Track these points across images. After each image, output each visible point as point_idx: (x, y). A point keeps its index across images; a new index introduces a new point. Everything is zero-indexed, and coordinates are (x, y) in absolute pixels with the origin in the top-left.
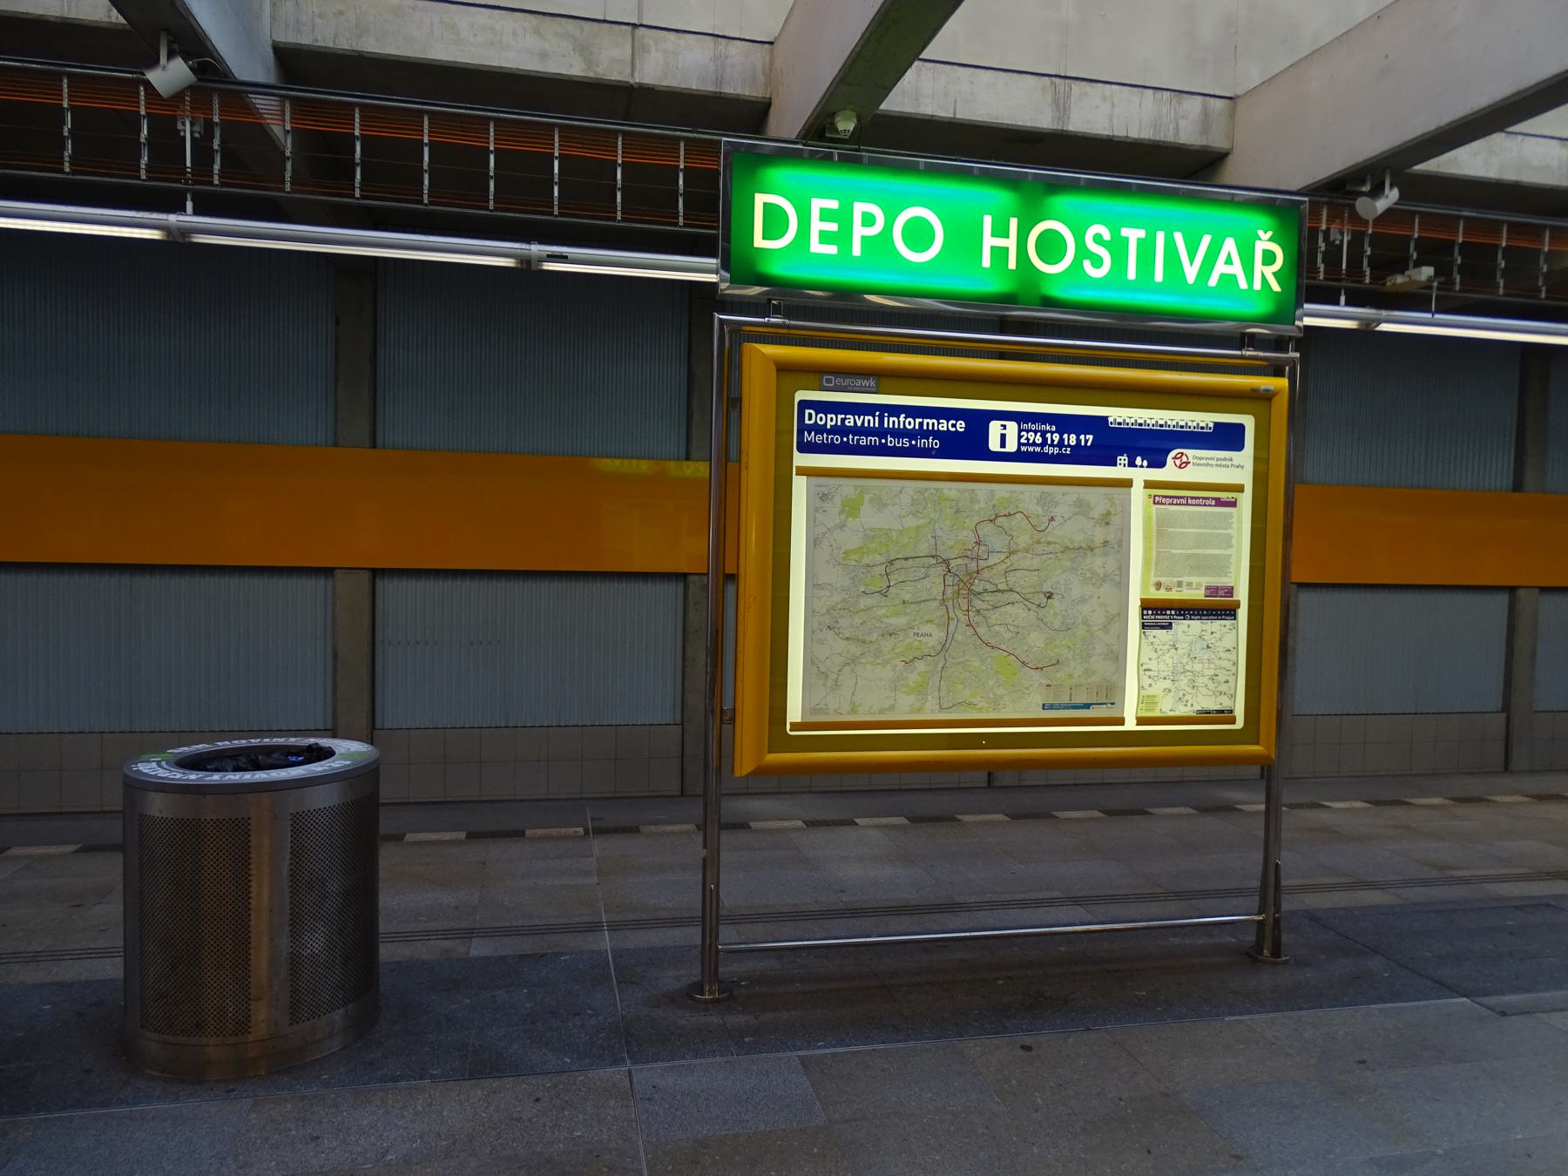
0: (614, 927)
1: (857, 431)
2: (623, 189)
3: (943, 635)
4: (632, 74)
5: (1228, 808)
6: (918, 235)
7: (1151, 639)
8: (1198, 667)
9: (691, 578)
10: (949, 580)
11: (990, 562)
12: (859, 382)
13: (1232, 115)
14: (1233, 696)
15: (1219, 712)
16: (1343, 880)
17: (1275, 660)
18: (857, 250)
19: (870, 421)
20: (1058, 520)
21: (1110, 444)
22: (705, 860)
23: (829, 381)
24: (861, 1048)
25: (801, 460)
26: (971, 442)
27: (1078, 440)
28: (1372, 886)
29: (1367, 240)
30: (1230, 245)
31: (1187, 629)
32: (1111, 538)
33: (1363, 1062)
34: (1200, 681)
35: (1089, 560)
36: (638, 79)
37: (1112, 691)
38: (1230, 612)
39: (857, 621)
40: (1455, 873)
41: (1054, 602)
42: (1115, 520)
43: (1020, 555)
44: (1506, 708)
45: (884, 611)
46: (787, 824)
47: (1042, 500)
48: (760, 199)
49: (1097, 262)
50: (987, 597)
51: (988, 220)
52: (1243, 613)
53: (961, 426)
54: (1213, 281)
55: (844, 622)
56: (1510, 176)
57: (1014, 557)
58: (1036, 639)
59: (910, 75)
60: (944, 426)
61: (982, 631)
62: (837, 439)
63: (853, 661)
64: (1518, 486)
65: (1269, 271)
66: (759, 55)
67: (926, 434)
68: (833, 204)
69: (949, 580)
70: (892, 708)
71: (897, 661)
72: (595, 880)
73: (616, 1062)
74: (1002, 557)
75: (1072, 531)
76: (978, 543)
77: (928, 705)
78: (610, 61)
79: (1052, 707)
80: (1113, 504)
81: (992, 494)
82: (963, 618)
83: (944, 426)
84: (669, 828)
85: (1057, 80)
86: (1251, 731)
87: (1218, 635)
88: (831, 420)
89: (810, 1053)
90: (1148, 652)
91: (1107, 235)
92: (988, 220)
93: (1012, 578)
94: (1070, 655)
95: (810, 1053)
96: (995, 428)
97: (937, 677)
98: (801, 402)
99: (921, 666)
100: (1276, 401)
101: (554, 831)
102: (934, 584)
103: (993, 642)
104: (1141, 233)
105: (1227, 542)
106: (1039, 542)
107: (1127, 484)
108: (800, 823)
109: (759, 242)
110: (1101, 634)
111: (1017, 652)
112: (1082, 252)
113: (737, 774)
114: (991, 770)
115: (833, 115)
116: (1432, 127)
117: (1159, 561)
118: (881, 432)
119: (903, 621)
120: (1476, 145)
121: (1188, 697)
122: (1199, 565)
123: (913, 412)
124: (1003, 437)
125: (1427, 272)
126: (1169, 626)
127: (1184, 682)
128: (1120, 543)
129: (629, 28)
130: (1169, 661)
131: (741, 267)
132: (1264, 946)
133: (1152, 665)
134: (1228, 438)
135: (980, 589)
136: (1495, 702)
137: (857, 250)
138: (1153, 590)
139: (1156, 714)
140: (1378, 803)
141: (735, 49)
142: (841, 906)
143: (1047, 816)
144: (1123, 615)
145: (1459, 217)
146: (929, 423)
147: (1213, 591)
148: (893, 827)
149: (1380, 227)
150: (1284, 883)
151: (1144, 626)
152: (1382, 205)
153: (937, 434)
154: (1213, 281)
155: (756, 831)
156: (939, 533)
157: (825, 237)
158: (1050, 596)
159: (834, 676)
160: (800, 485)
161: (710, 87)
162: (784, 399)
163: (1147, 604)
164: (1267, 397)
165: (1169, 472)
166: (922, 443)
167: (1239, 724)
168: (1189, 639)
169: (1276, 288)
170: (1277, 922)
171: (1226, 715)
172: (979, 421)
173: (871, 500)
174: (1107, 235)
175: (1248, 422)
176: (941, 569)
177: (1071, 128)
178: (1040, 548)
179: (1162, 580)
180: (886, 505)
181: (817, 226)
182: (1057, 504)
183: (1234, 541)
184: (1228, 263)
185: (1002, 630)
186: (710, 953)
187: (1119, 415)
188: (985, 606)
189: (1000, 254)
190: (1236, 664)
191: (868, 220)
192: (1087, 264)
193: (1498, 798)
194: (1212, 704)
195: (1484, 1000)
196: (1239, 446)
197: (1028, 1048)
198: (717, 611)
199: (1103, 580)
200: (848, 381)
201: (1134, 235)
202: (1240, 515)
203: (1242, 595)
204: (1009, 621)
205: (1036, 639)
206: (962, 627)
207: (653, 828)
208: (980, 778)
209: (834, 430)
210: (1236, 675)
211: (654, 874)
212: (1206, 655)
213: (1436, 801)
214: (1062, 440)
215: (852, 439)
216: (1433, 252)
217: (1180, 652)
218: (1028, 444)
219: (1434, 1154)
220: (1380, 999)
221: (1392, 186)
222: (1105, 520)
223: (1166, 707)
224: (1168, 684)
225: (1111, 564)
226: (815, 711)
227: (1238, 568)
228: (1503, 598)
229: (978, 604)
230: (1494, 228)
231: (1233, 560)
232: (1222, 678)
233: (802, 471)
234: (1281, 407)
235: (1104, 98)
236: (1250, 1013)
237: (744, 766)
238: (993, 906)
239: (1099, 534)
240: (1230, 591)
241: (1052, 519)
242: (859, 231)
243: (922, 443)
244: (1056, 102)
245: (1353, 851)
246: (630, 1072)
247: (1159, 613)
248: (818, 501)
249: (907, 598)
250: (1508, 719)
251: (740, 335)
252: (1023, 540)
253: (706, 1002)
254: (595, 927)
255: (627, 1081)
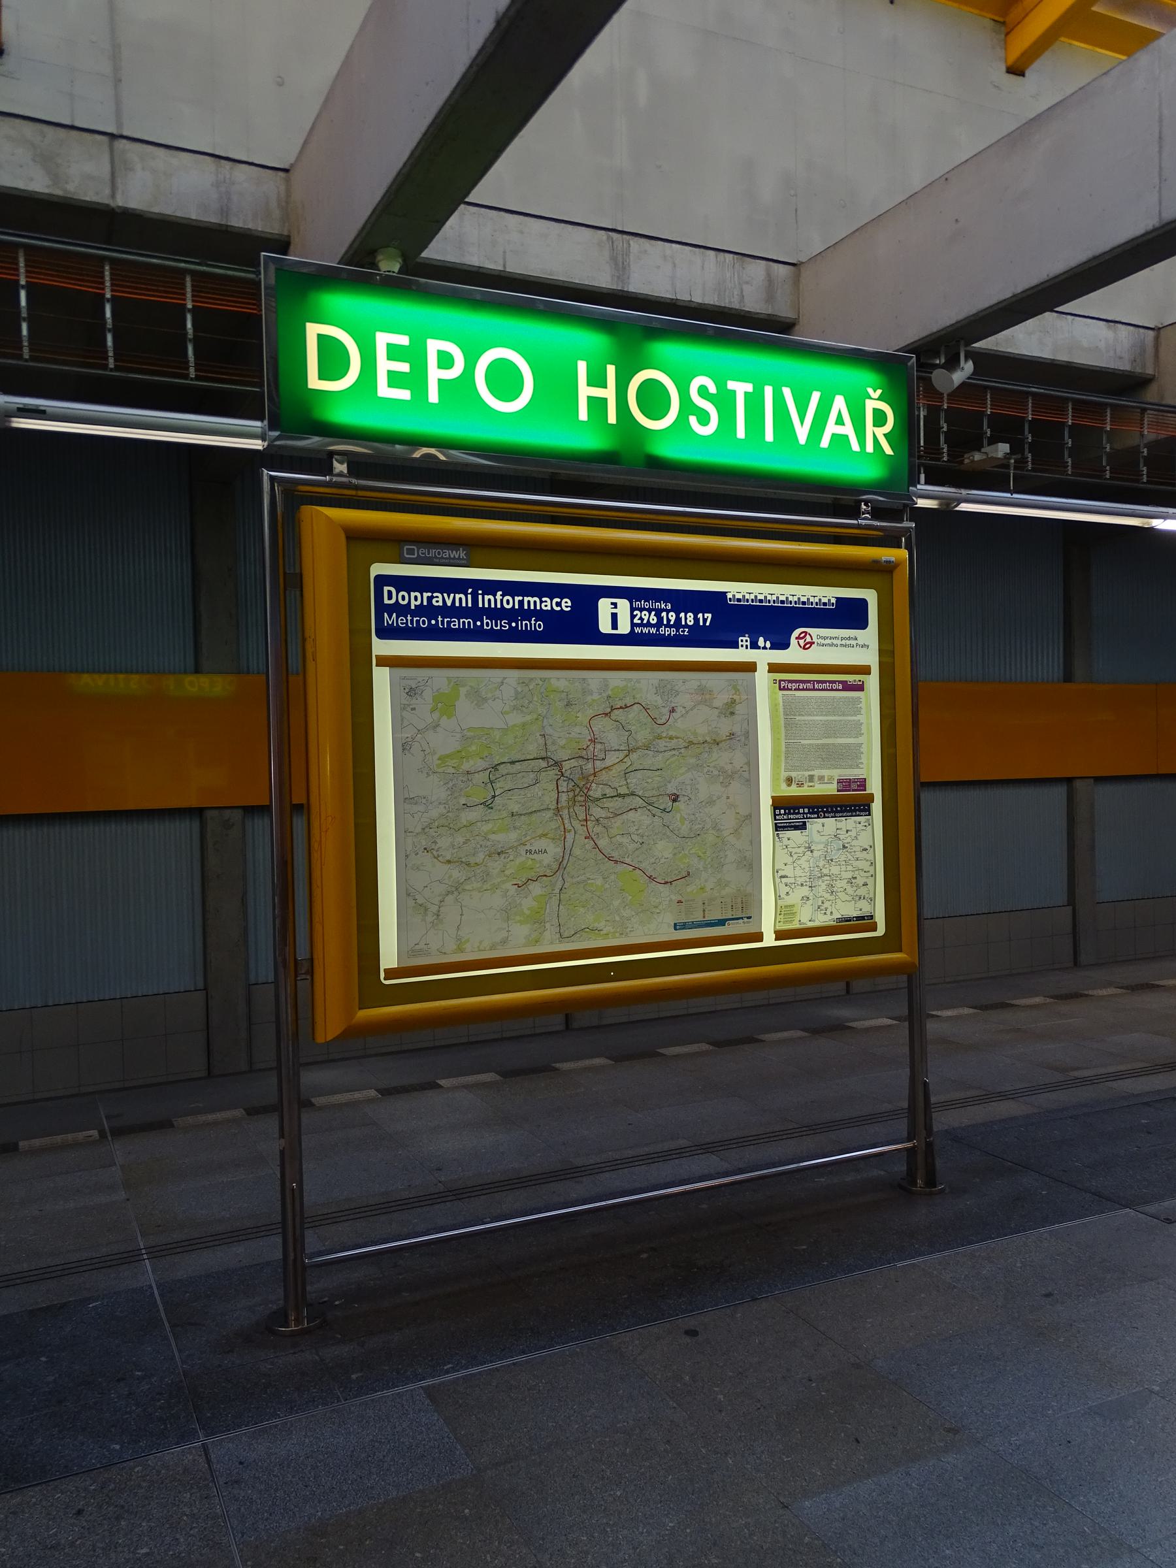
0: (156, 1253)
1: (445, 611)
2: (116, 332)
3: (559, 850)
4: (113, 196)
5: (839, 1028)
6: (504, 380)
7: (785, 842)
8: (835, 870)
9: (209, 814)
10: (563, 786)
11: (608, 762)
12: (447, 553)
13: (796, 280)
14: (872, 900)
15: (859, 918)
16: (970, 1093)
17: (908, 862)
18: (433, 396)
19: (462, 599)
20: (679, 709)
21: (731, 623)
22: (282, 1152)
23: (411, 552)
24: (498, 1364)
25: (382, 647)
26: (578, 624)
27: (696, 620)
28: (1003, 1096)
29: (942, 415)
30: (839, 403)
31: (822, 828)
32: (736, 729)
33: (1048, 1295)
34: (840, 884)
35: (715, 755)
36: (120, 202)
37: (748, 905)
38: (862, 807)
39: (460, 839)
40: (1077, 1074)
41: (680, 805)
42: (739, 709)
43: (639, 752)
44: (1071, 901)
45: (490, 826)
46: (357, 1095)
47: (661, 689)
48: (313, 330)
49: (704, 419)
50: (607, 803)
51: (582, 367)
52: (877, 807)
53: (566, 604)
54: (825, 442)
55: (444, 842)
56: (1063, 357)
57: (634, 756)
58: (663, 849)
59: (452, 221)
60: (547, 604)
61: (602, 843)
62: (424, 623)
63: (457, 888)
64: (1068, 677)
65: (880, 432)
66: (272, 185)
67: (527, 614)
68: (404, 340)
69: (563, 786)
70: (504, 942)
71: (508, 885)
72: (122, 1195)
73: (185, 1436)
74: (621, 755)
75: (697, 722)
76: (593, 741)
77: (547, 934)
78: (83, 177)
79: (684, 926)
80: (737, 690)
81: (605, 684)
82: (582, 830)
83: (547, 604)
84: (211, 1117)
85: (614, 235)
86: (891, 941)
87: (853, 834)
88: (416, 599)
89: (436, 1381)
90: (783, 856)
91: (713, 389)
92: (582, 367)
93: (633, 779)
94: (701, 867)
95: (436, 1381)
96: (604, 605)
97: (554, 901)
98: (378, 577)
99: (536, 889)
100: (897, 575)
101: (58, 1139)
102: (546, 792)
103: (616, 855)
104: (749, 387)
105: (856, 729)
106: (659, 737)
107: (751, 667)
108: (373, 1093)
109: (314, 382)
110: (732, 839)
111: (642, 866)
112: (688, 407)
113: (320, 1038)
114: (567, 1010)
115: (373, 253)
116: (1008, 295)
117: (789, 753)
118: (475, 612)
119: (513, 836)
120: (1030, 323)
121: (827, 904)
122: (831, 756)
123: (511, 588)
124: (614, 617)
125: (1003, 448)
126: (803, 827)
127: (822, 885)
128: (747, 735)
129: (104, 139)
130: (805, 865)
131: (289, 413)
132: (918, 1176)
133: (788, 871)
134: (849, 615)
135: (598, 794)
136: (1062, 898)
137: (433, 396)
138: (784, 786)
139: (795, 925)
140: (984, 1008)
141: (242, 174)
142: (441, 1188)
143: (650, 1054)
144: (752, 818)
145: (1028, 393)
146: (531, 601)
147: (845, 784)
148: (484, 1085)
149: (969, 399)
150: (933, 1099)
151: (777, 828)
152: (958, 377)
153: (540, 614)
154: (825, 442)
155: (320, 1108)
156: (549, 730)
157: (395, 379)
158: (675, 799)
159: (434, 909)
160: (382, 678)
161: (213, 218)
162: (357, 573)
163: (781, 804)
164: (885, 570)
165: (793, 654)
166: (523, 625)
167: (881, 931)
168: (824, 839)
169: (889, 451)
170: (929, 1145)
171: (865, 921)
172: (587, 598)
173: (467, 695)
174: (713, 389)
175: (870, 596)
176: (553, 773)
177: (632, 289)
178: (662, 744)
179: (793, 774)
180: (485, 700)
181: (384, 366)
182: (677, 693)
183: (864, 729)
184: (832, 424)
185: (625, 840)
186: (294, 1270)
187: (738, 590)
188: (603, 813)
189: (598, 405)
190: (873, 864)
191: (445, 361)
192: (693, 420)
193: (1095, 992)
194: (851, 910)
195: (1150, 1209)
196: (862, 624)
197: (692, 1333)
198: (280, 835)
199: (731, 777)
200: (433, 552)
201: (741, 388)
202: (868, 698)
203: (875, 787)
204: (633, 829)
205: (663, 849)
206: (581, 839)
207: (190, 1120)
208: (557, 1022)
209: (420, 610)
210: (874, 876)
211: (208, 1178)
212: (842, 856)
213: (1037, 1000)
214: (678, 619)
215: (441, 621)
216: (1005, 429)
217: (816, 854)
218: (641, 625)
219: (1152, 1392)
220: (1046, 1221)
221: (966, 360)
222: (729, 710)
223: (806, 917)
224: (805, 891)
225: (739, 759)
226: (414, 953)
227: (870, 758)
228: (1060, 791)
229: (597, 812)
230: (1059, 405)
231: (864, 749)
232: (860, 881)
233: (384, 661)
234: (902, 579)
235: (665, 257)
236: (921, 1254)
237: (329, 1025)
238: (616, 1165)
239: (725, 727)
240: (862, 784)
241: (673, 710)
242: (435, 374)
243: (523, 625)
244: (614, 259)
245: (1004, 1058)
246: (205, 1448)
247: (793, 812)
248: (405, 697)
249: (516, 808)
250: (1074, 910)
251: (295, 499)
252: (643, 735)
253: (293, 1334)
254: (131, 1258)
255: (202, 1460)
